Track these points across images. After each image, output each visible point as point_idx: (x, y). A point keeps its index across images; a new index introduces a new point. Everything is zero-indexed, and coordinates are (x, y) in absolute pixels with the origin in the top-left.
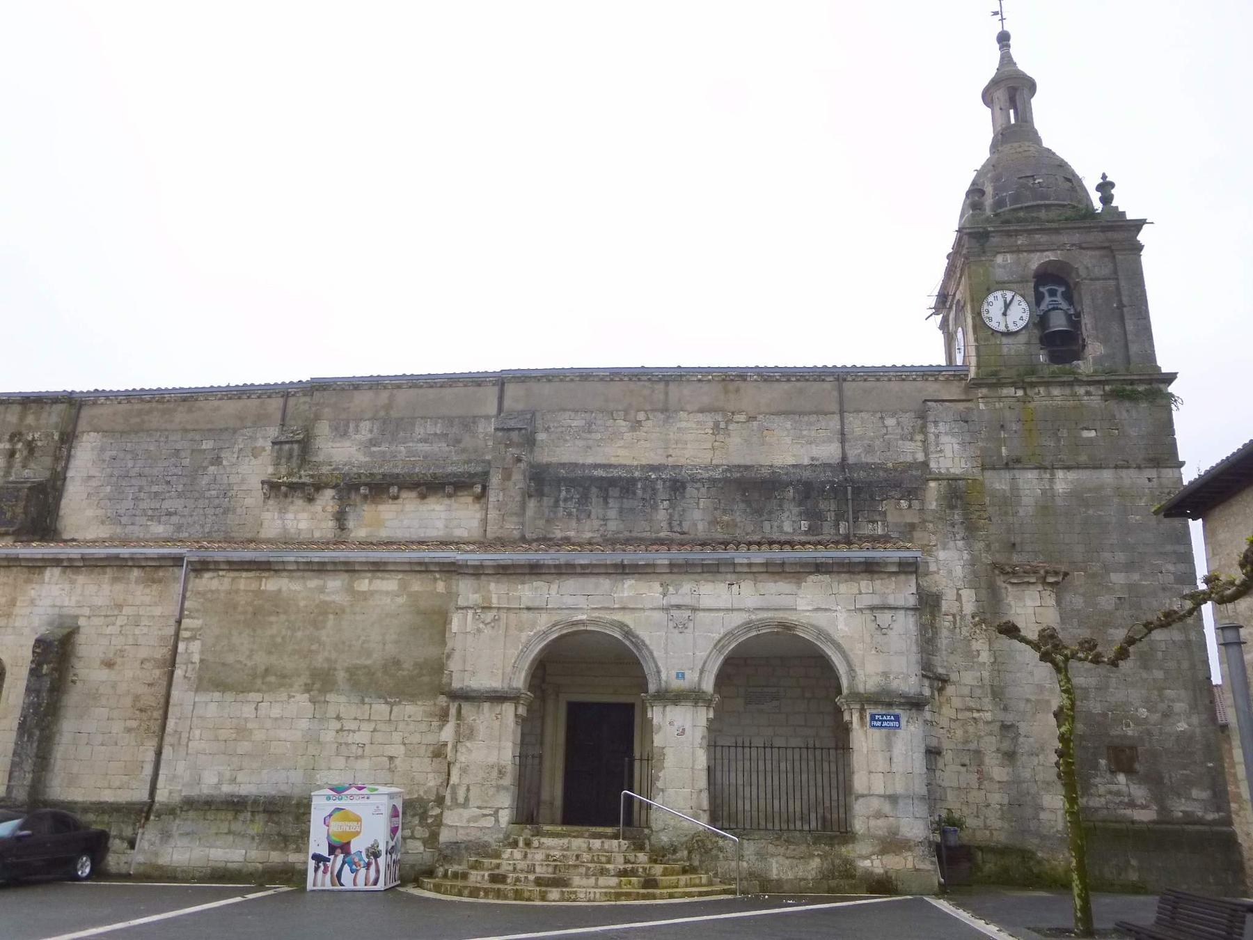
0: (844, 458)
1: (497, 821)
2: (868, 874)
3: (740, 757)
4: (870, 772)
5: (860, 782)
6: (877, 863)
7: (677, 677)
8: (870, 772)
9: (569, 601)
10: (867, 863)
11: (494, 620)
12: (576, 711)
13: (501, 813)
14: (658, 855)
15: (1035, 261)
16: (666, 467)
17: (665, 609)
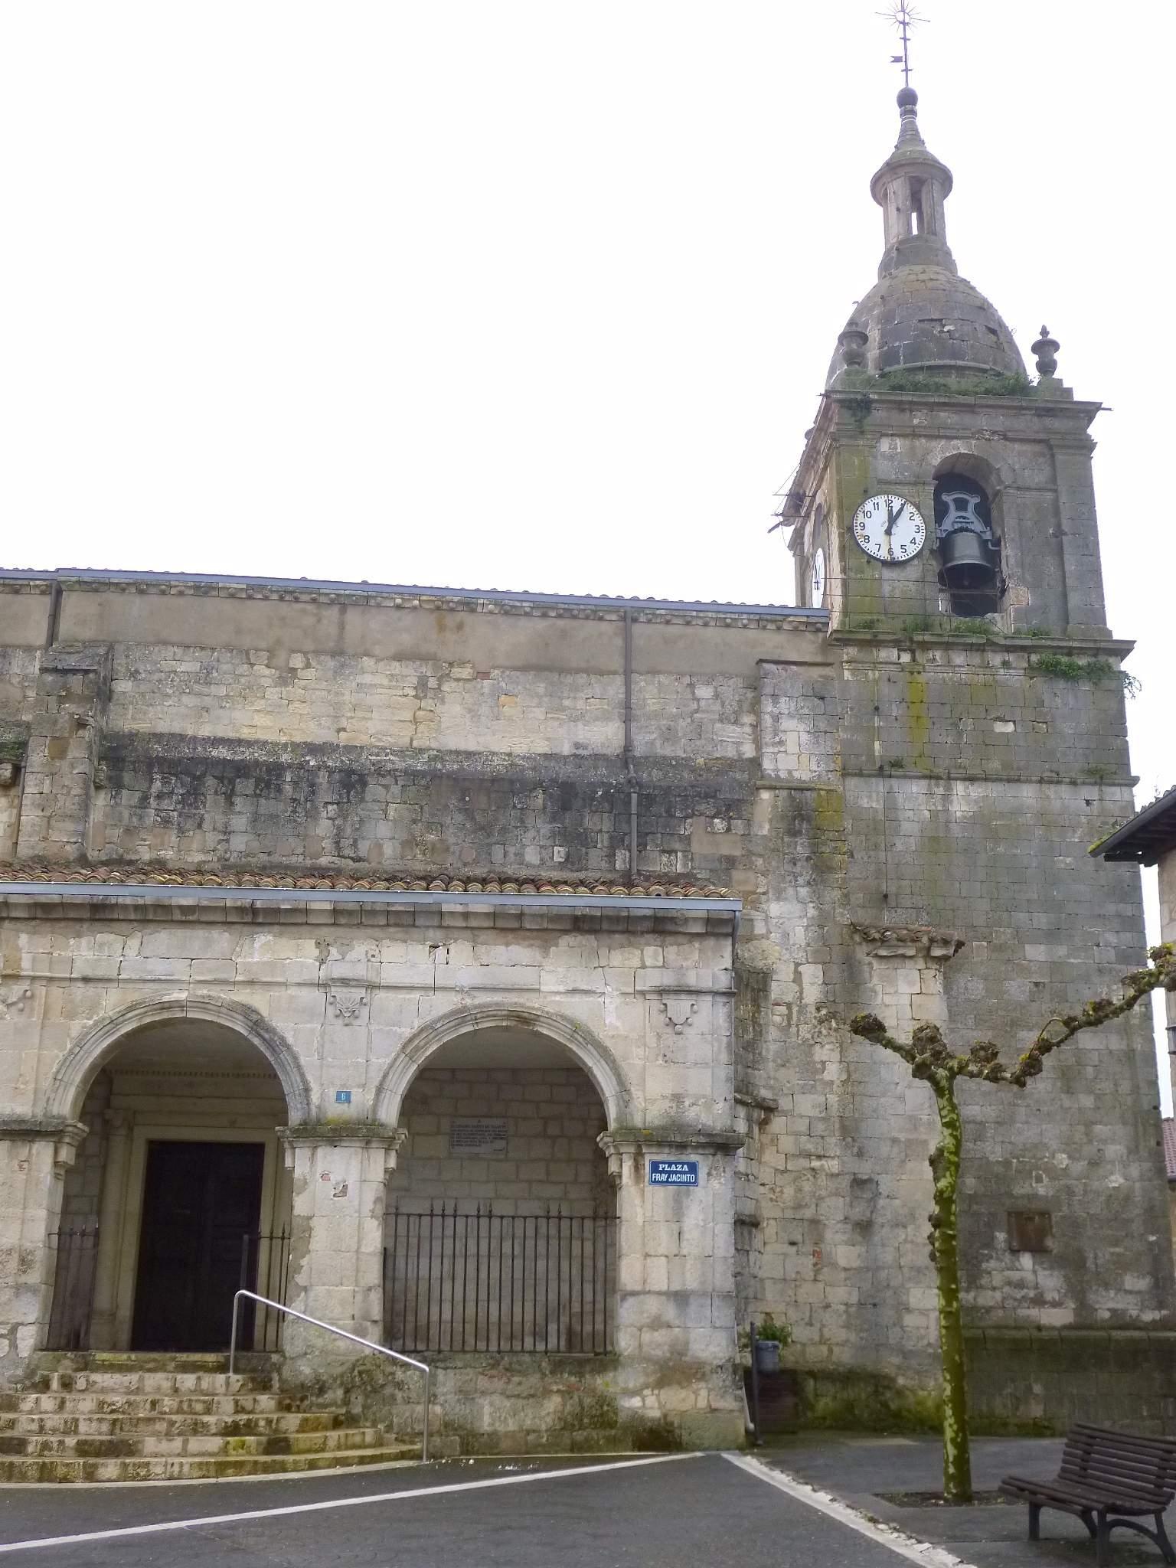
0: (628, 747)
1: (13, 1345)
2: (636, 1418)
3: (437, 1232)
4: (647, 1256)
5: (629, 1273)
6: (651, 1401)
7: (338, 1099)
10: (636, 1402)
11: (24, 998)
12: (161, 1154)
13: (22, 1332)
15: (939, 453)
17: (323, 985)
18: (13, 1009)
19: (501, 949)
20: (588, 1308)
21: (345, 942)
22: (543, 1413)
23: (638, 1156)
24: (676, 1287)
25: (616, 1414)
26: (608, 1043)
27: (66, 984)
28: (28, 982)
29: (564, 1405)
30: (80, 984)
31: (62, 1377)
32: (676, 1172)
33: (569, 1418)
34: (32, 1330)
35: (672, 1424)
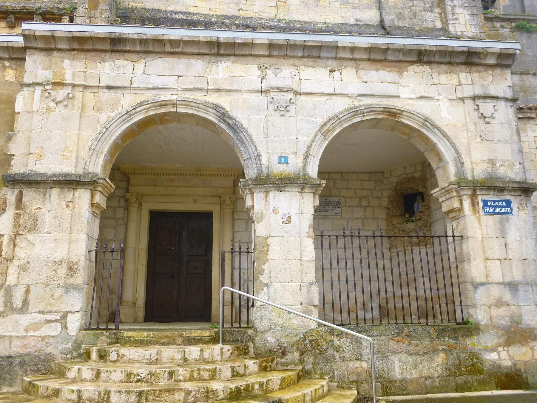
0: (382, 21)
1: (65, 327)
2: (496, 366)
4: (487, 259)
5: (475, 270)
6: (504, 355)
7: (280, 162)
8: (487, 259)
9: (158, 82)
10: (494, 356)
11: (67, 98)
12: (156, 218)
13: (70, 318)
14: (268, 360)
16: (238, 18)
18: (61, 106)
19: (374, 72)
20: (390, 295)
21: (277, 67)
22: (435, 365)
23: (473, 197)
24: (508, 279)
25: (482, 365)
26: (445, 129)
27: (96, 90)
28: (70, 88)
29: (448, 359)
30: (105, 91)
31: (99, 350)
32: (499, 207)
33: (452, 369)
34: (78, 316)
35: (520, 370)
